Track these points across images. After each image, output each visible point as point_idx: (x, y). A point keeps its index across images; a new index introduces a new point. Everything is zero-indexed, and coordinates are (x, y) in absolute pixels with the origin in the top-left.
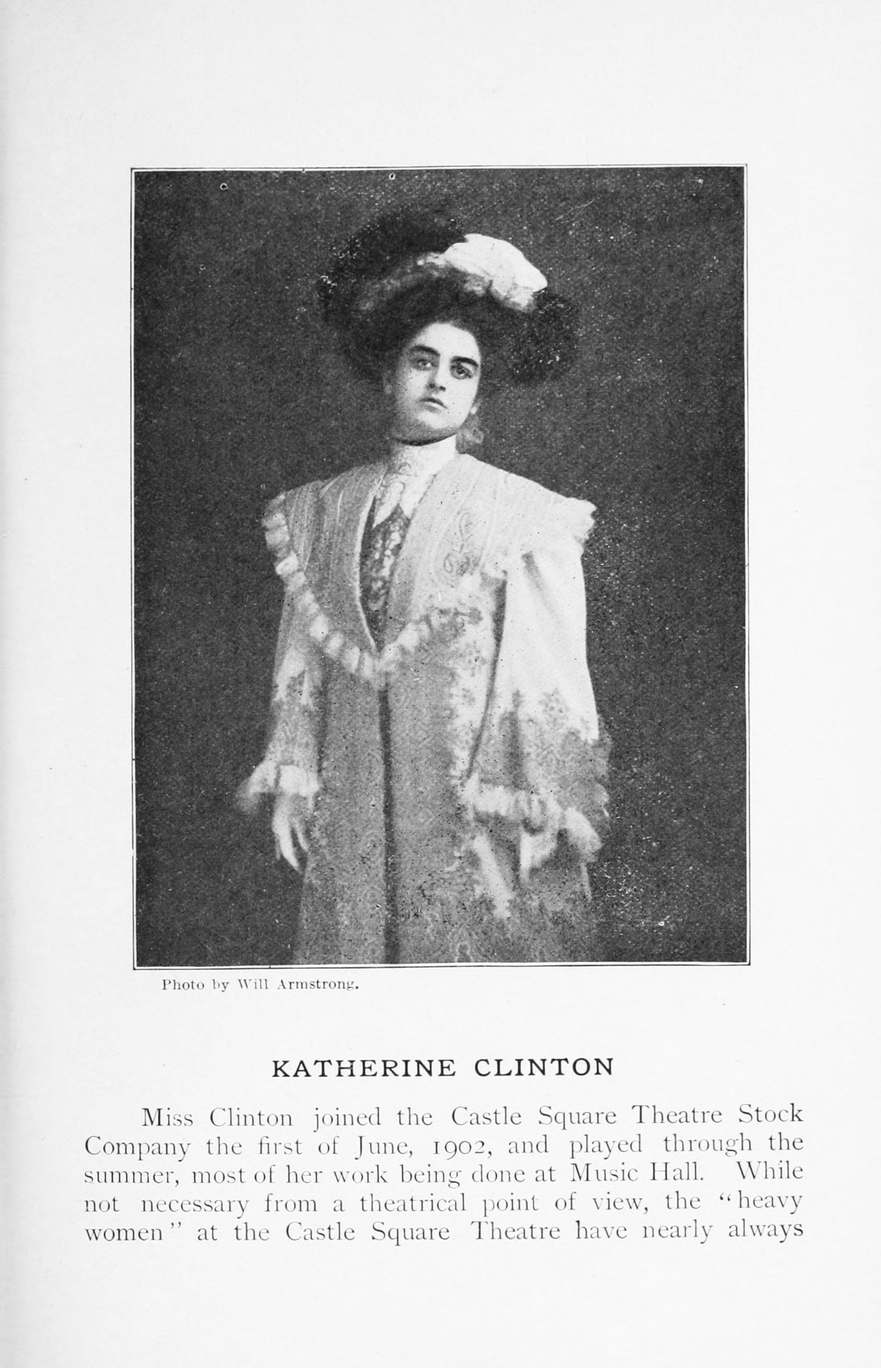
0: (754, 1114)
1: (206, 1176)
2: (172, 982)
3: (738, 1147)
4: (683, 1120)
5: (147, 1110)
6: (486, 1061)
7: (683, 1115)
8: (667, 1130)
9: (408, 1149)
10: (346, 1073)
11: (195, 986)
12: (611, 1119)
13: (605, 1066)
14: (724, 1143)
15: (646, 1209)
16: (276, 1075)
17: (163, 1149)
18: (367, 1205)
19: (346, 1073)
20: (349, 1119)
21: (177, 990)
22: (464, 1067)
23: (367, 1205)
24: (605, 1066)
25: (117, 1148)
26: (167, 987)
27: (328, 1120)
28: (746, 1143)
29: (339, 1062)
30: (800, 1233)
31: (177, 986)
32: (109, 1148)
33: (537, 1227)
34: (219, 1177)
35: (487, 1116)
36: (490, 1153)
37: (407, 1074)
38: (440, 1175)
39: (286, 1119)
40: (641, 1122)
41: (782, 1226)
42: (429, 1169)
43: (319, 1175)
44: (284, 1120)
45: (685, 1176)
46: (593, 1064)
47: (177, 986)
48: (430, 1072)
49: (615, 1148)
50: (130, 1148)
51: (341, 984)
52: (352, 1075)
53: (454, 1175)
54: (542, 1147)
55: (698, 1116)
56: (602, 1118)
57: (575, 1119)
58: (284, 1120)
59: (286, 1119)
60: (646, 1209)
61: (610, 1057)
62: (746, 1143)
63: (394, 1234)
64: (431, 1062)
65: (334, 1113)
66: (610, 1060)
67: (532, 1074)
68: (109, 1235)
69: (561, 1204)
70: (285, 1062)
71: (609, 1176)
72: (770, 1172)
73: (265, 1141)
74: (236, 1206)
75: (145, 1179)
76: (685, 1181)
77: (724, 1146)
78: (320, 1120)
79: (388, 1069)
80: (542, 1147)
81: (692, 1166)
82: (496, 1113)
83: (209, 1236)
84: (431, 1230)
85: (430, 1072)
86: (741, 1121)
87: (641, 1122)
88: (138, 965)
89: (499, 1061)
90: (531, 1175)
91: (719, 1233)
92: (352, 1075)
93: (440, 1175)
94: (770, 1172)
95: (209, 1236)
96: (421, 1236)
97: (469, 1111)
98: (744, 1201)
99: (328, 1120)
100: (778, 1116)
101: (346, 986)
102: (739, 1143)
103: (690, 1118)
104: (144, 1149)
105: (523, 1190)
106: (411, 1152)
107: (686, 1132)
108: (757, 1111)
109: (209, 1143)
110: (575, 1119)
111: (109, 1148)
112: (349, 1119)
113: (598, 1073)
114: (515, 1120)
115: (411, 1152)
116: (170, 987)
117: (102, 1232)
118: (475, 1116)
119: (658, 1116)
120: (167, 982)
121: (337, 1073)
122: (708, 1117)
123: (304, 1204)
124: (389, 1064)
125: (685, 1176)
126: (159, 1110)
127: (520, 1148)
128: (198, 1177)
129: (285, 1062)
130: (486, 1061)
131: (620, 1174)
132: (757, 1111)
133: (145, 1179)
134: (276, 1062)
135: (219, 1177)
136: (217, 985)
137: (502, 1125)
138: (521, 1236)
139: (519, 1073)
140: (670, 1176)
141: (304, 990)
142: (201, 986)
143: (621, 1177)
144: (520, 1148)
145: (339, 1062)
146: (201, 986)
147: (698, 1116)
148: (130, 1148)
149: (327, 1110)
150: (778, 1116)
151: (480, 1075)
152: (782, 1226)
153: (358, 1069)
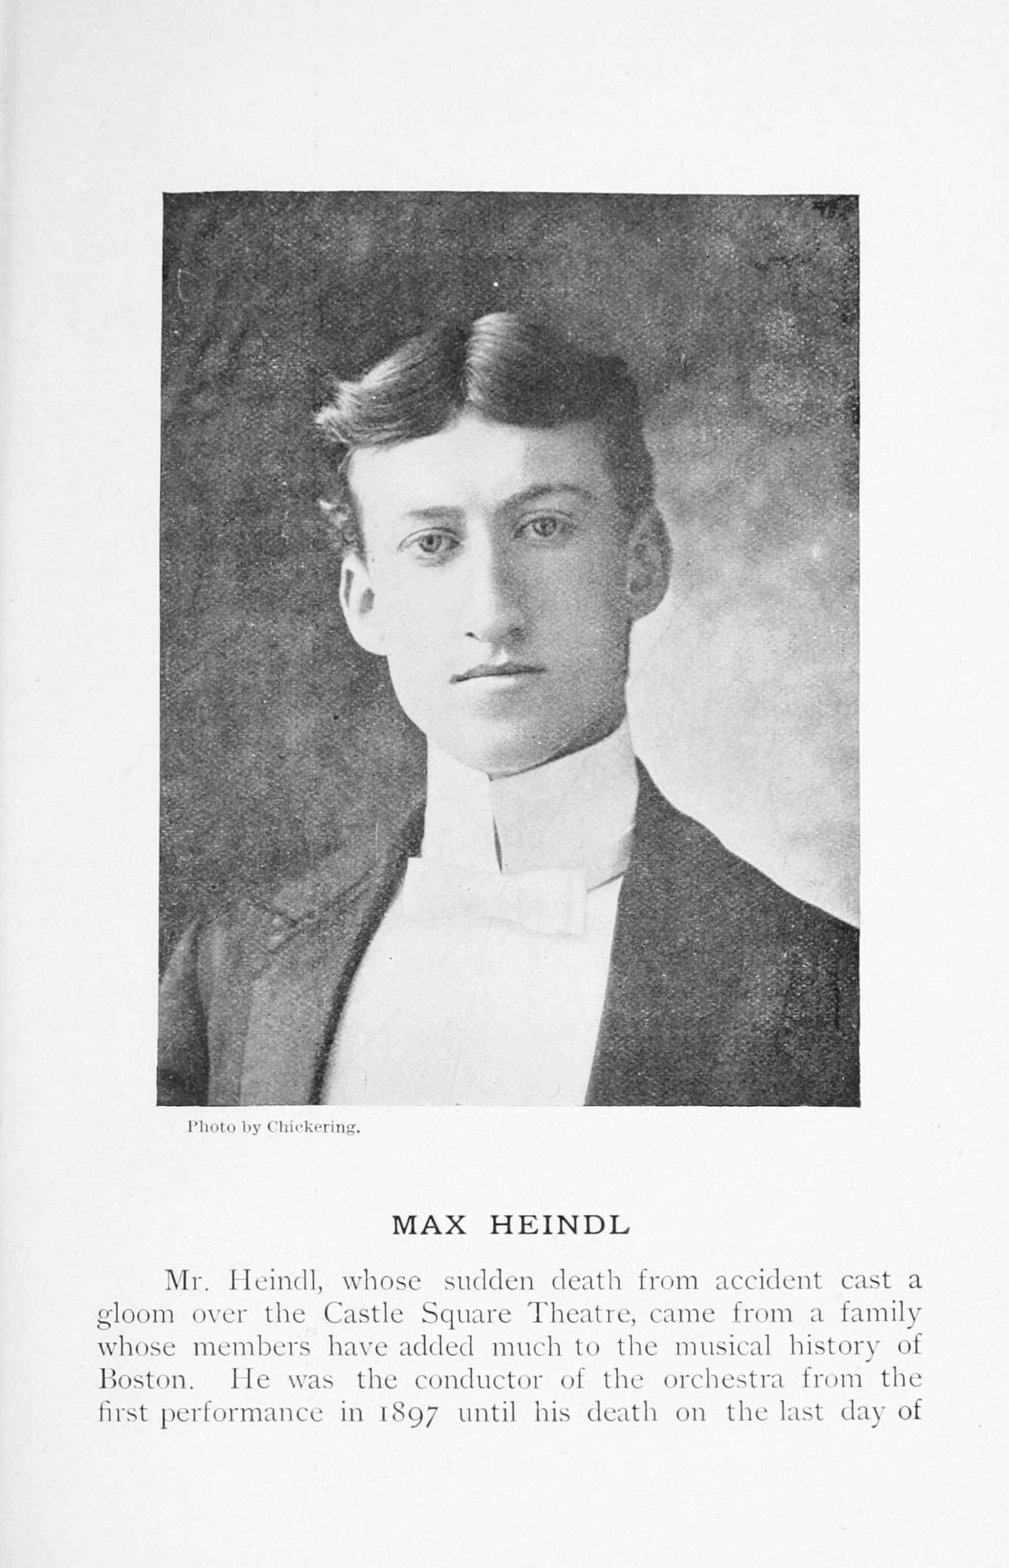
1: (209, 1347)
2: (199, 1124)
3: (111, 1319)
7: (588, 1280)
9: (630, 1317)
10: (502, 1229)
11: (225, 1127)
16: (495, 1232)
18: (890, 1379)
19: (502, 1229)
21: (284, 1133)
22: (477, 1224)
23: (890, 1379)
26: (193, 1129)
30: (566, 1418)
34: (142, 1349)
35: (364, 1313)
41: (875, 1408)
45: (764, 1350)
48: (574, 1230)
51: (341, 1128)
52: (509, 1232)
56: (495, 1316)
57: (464, 1317)
63: (447, 1316)
64: (575, 1217)
65: (269, 1275)
67: (561, 1232)
69: (568, 1382)
70: (461, 1217)
71: (716, 1349)
72: (797, 1347)
73: (106, 1406)
75: (209, 1350)
76: (765, 1356)
85: (574, 1230)
86: (424, 1321)
90: (394, 1349)
91: (889, 1415)
94: (797, 1347)
95: (630, 1416)
96: (478, 1319)
101: (346, 1129)
102: (113, 1314)
105: (693, 1365)
106: (634, 1321)
110: (464, 1317)
114: (396, 1317)
115: (634, 1321)
120: (193, 1124)
121: (492, 1230)
123: (778, 1314)
127: (865, 1315)
128: (201, 1348)
129: (461, 1217)
131: (728, 1347)
133: (209, 1350)
134: (494, 1217)
135: (142, 1349)
138: (623, 1417)
139: (548, 1232)
141: (341, 1134)
142: (231, 1128)
143: (729, 1351)
144: (865, 1315)
146: (231, 1128)
147: (603, 1315)
152: (875, 1408)
153: (516, 1225)
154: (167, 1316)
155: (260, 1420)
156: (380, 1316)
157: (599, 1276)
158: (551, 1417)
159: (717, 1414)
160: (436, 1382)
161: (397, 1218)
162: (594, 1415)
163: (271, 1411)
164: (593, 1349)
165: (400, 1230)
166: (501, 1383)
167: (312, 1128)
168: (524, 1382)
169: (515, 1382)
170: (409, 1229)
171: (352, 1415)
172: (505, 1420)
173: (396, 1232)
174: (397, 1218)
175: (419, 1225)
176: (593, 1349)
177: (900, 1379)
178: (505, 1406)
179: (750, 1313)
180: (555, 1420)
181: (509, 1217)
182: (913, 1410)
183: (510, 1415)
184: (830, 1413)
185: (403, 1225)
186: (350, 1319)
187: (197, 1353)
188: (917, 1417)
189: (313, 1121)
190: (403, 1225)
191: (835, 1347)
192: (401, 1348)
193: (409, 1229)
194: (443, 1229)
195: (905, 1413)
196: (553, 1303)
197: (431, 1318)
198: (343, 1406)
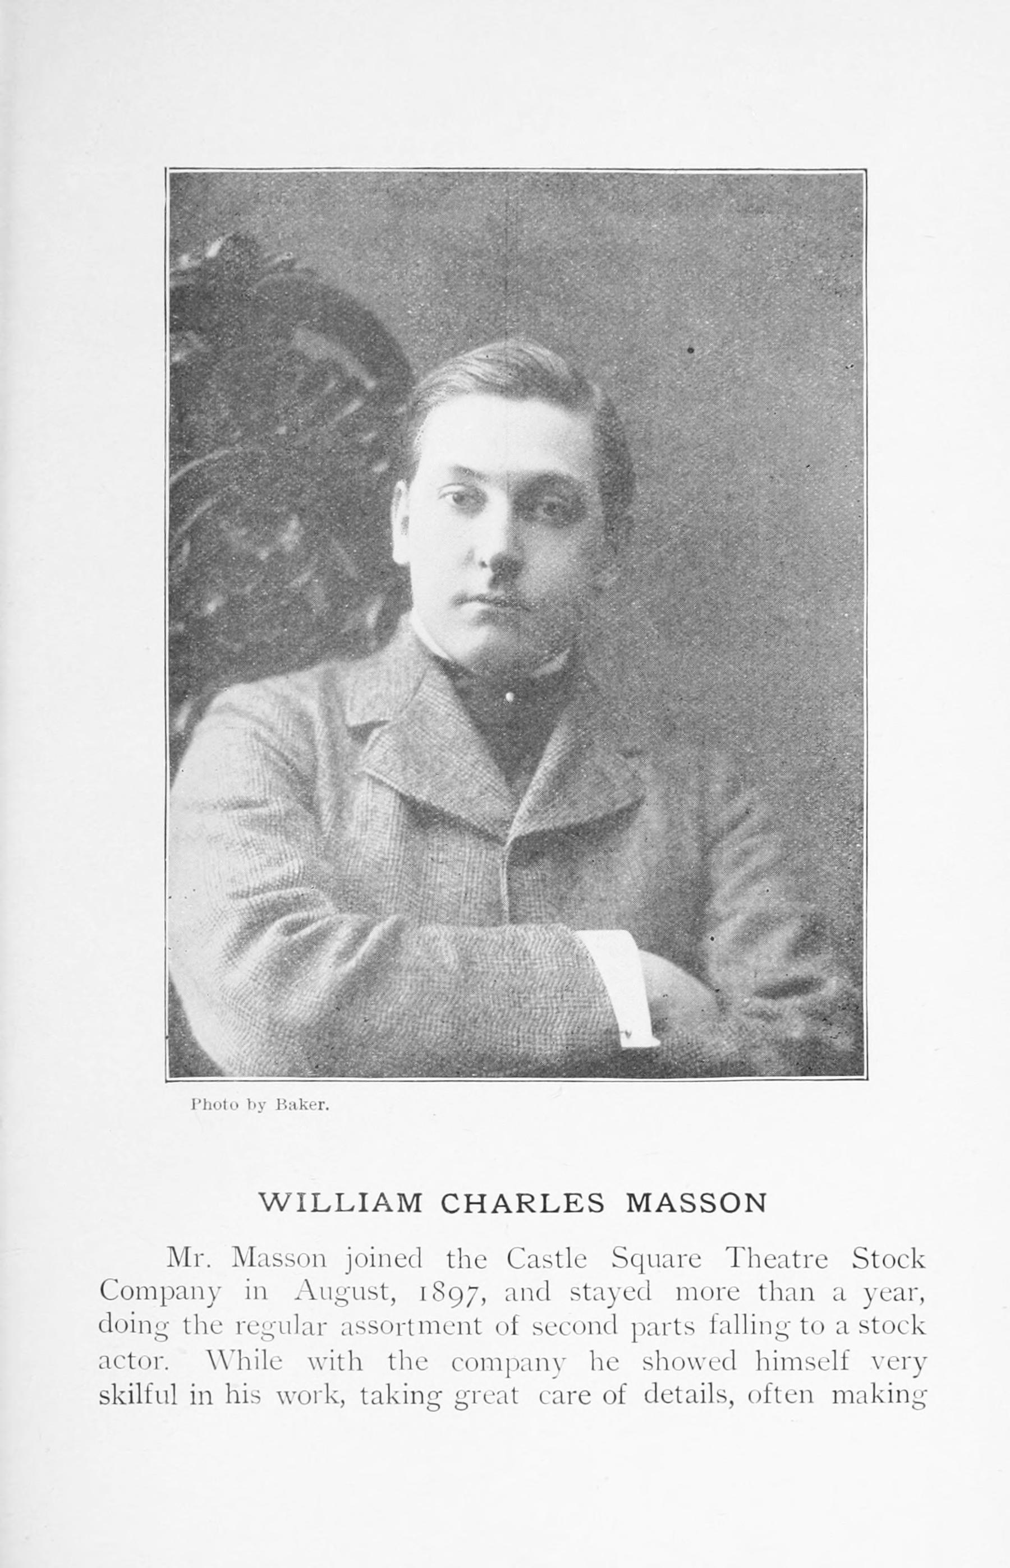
0: (871, 1259)
1: (692, 1292)
4: (783, 1264)
5: (173, 1248)
6: (455, 1195)
7: (783, 1258)
8: (764, 1276)
10: (475, 1208)
11: (228, 1105)
12: (821, 1263)
13: (757, 1202)
14: (334, 1291)
15: (484, 1300)
17: (189, 1294)
19: (475, 1208)
20: (385, 1260)
24: (757, 1202)
25: (135, 1293)
27: (361, 1260)
28: (355, 1362)
29: (468, 1196)
31: (208, 1107)
32: (127, 1293)
33: (683, 1388)
36: (393, 1300)
37: (363, 1209)
38: (766, 1326)
39: (319, 1259)
40: (735, 1265)
42: (133, 1317)
43: (323, 1326)
44: (317, 1260)
45: (733, 1329)
46: (744, 1200)
47: (208, 1107)
49: (876, 1297)
50: (151, 1292)
52: (482, 1211)
53: (781, 1325)
54: (543, 1294)
55: (801, 1261)
56: (685, 1261)
57: (654, 1262)
58: (317, 1260)
59: (319, 1259)
60: (484, 1300)
61: (468, 1193)
62: (355, 1362)
65: (368, 1253)
66: (763, 1195)
68: (305, 1398)
71: (367, 1294)
74: (911, 1363)
77: (334, 1294)
78: (352, 1261)
79: (524, 1204)
80: (543, 1294)
81: (741, 1319)
82: (558, 1255)
83: (510, 1399)
84: (570, 1393)
86: (855, 1266)
87: (735, 1265)
88: (862, 1074)
89: (545, 1196)
91: (597, 1397)
92: (482, 1211)
93: (766, 1326)
95: (510, 1399)
97: (527, 1253)
98: (597, 1363)
99: (361, 1260)
100: (897, 1261)
102: (350, 1291)
103: (791, 1263)
104: (168, 1293)
107: (788, 1279)
108: (874, 1255)
109: (761, 1288)
110: (654, 1262)
111: (127, 1293)
112: (385, 1260)
113: (749, 1210)
116: (199, 1107)
117: (297, 1395)
118: (533, 1258)
119: (755, 1260)
120: (197, 1101)
122: (811, 1261)
124: (525, 1199)
125: (733, 1329)
126: (252, 1248)
128: (683, 1293)
130: (455, 1195)
132: (874, 1255)
136: (252, 1105)
137: (456, 1268)
140: (717, 1330)
145: (468, 1196)
147: (801, 1261)
148: (151, 1292)
149: (361, 1248)
150: (897, 1261)
151: (446, 1210)
154: (162, 1295)
155: (852, 1402)
156: (564, 1261)
157: (795, 1255)
158: (241, 1399)
159: (823, 1397)
160: (472, 1364)
161: (631, 1196)
162: (651, 1396)
163: (378, 1394)
164: (818, 1328)
165: (634, 1207)
166: (124, 1363)
167: (307, 1105)
168: (145, 1363)
169: (135, 1364)
170: (643, 1207)
171: (201, 1397)
172: (891, 1401)
173: (631, 1210)
174: (262, 1194)
175: (654, 1203)
176: (818, 1328)
177: (406, 1362)
178: (130, 1388)
179: (810, 1259)
180: (711, 1401)
181: (482, 1196)
182: (764, 1395)
183: (806, 1396)
184: (527, 1396)
185: (275, 1202)
186: (533, 1264)
187: (421, 1332)
188: (621, 1402)
189: (308, 1099)
190: (275, 1202)
191: (879, 1327)
192: (343, 1328)
193: (643, 1207)
194: (676, 1207)
195: (610, 1397)
196: (711, 1384)
197: (621, 1262)
198: (193, 1389)
